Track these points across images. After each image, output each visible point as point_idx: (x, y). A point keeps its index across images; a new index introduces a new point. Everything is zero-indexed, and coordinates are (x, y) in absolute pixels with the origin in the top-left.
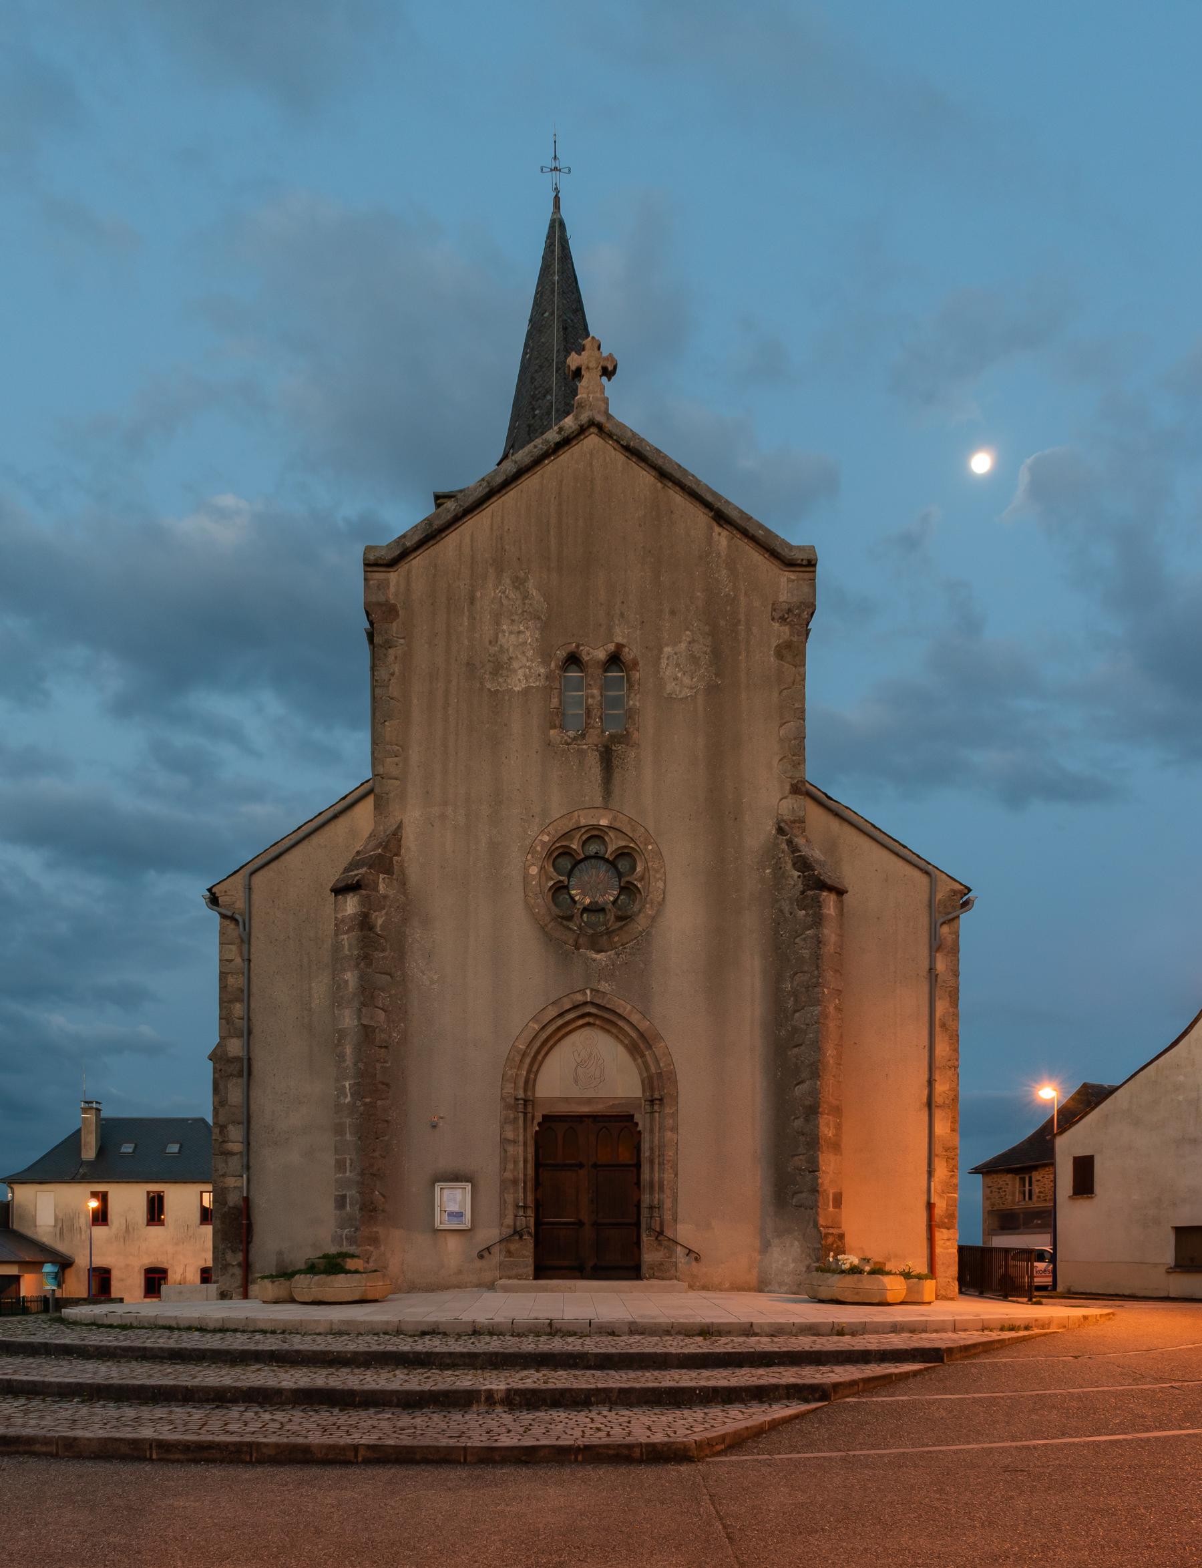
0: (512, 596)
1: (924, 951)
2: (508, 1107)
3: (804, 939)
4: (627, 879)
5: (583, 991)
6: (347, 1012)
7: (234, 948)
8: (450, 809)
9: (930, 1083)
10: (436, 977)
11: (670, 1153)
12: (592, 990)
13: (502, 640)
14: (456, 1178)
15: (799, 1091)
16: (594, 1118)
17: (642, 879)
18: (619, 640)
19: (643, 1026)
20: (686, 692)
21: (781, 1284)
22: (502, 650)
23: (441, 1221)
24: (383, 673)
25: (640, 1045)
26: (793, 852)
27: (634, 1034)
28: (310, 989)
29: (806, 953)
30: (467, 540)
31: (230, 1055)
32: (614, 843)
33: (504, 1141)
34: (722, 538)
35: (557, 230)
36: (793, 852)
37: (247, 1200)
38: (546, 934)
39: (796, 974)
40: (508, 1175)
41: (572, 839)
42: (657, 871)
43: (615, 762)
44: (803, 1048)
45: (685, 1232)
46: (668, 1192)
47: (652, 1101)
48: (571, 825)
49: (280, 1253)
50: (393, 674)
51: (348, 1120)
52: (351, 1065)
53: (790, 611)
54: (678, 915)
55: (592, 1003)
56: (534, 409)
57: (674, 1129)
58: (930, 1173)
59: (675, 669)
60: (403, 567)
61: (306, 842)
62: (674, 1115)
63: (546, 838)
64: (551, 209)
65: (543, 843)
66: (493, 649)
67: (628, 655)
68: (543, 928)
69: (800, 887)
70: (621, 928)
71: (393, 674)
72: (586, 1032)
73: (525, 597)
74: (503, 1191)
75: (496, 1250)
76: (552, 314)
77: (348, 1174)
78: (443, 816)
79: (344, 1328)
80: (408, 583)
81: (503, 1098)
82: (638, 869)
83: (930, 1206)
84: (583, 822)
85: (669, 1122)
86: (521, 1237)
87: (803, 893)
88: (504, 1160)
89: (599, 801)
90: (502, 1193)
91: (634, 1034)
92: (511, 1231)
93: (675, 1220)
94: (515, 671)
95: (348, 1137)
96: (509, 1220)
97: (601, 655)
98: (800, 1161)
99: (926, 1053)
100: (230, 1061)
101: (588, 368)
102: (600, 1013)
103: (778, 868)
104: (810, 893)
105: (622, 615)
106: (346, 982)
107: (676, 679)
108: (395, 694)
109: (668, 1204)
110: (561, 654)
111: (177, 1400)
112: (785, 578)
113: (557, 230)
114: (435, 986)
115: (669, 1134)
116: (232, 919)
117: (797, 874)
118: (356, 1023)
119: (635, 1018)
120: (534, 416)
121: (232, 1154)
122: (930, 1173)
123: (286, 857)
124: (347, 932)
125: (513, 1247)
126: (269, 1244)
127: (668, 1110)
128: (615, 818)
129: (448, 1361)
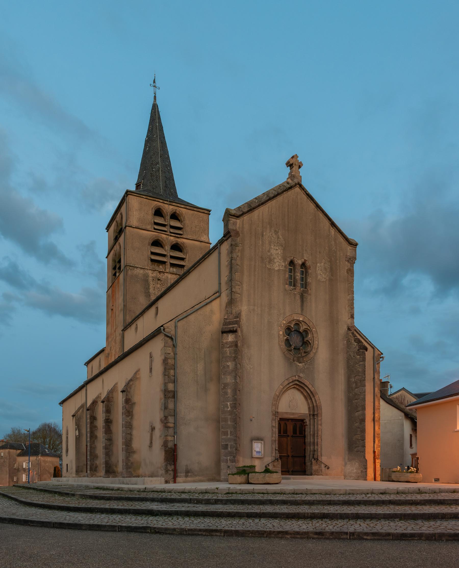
0: (274, 236)
3: (359, 365)
5: (295, 376)
6: (228, 377)
7: (170, 349)
8: (256, 307)
9: (374, 413)
10: (252, 367)
11: (320, 433)
12: (298, 376)
13: (272, 252)
14: (258, 439)
15: (357, 414)
16: (292, 420)
18: (305, 258)
19: (312, 389)
20: (324, 280)
21: (351, 477)
22: (271, 255)
23: (20, 459)
24: (234, 255)
25: (309, 396)
26: (354, 337)
27: (309, 392)
28: (197, 367)
29: (360, 370)
30: (261, 214)
31: (169, 389)
33: (273, 426)
34: (333, 231)
36: (354, 337)
37: (175, 445)
38: (285, 355)
39: (356, 376)
40: (274, 439)
43: (304, 299)
45: (324, 459)
47: (314, 415)
48: (292, 319)
49: (187, 466)
50: (238, 256)
51: (229, 417)
53: (350, 259)
54: (322, 353)
55: (298, 380)
56: (152, 168)
57: (321, 425)
58: (374, 442)
59: (319, 272)
60: (241, 219)
62: (321, 420)
63: (285, 322)
65: (284, 324)
66: (269, 254)
67: (308, 264)
68: (284, 353)
69: (357, 348)
71: (238, 256)
73: (278, 238)
74: (272, 444)
75: (270, 465)
76: (157, 136)
77: (229, 436)
78: (254, 310)
79: (351, 492)
80: (243, 224)
81: (272, 412)
82: (309, 337)
83: (374, 452)
84: (295, 318)
85: (319, 422)
86: (278, 460)
87: (358, 350)
89: (300, 312)
90: (272, 445)
92: (274, 458)
93: (321, 455)
94: (275, 263)
95: (229, 423)
96: (274, 455)
97: (300, 262)
99: (372, 404)
100: (169, 392)
101: (295, 164)
102: (300, 384)
103: (348, 341)
104: (361, 350)
105: (306, 250)
106: (228, 366)
107: (321, 275)
108: (239, 264)
109: (319, 450)
110: (289, 260)
111: (439, 518)
112: (349, 248)
114: (251, 370)
115: (319, 426)
117: (356, 344)
118: (233, 381)
119: (310, 387)
120: (153, 171)
121: (170, 427)
122: (374, 442)
123: (190, 317)
124: (228, 347)
125: (275, 464)
126: (183, 461)
127: (319, 418)
128: (304, 318)
129: (449, 502)
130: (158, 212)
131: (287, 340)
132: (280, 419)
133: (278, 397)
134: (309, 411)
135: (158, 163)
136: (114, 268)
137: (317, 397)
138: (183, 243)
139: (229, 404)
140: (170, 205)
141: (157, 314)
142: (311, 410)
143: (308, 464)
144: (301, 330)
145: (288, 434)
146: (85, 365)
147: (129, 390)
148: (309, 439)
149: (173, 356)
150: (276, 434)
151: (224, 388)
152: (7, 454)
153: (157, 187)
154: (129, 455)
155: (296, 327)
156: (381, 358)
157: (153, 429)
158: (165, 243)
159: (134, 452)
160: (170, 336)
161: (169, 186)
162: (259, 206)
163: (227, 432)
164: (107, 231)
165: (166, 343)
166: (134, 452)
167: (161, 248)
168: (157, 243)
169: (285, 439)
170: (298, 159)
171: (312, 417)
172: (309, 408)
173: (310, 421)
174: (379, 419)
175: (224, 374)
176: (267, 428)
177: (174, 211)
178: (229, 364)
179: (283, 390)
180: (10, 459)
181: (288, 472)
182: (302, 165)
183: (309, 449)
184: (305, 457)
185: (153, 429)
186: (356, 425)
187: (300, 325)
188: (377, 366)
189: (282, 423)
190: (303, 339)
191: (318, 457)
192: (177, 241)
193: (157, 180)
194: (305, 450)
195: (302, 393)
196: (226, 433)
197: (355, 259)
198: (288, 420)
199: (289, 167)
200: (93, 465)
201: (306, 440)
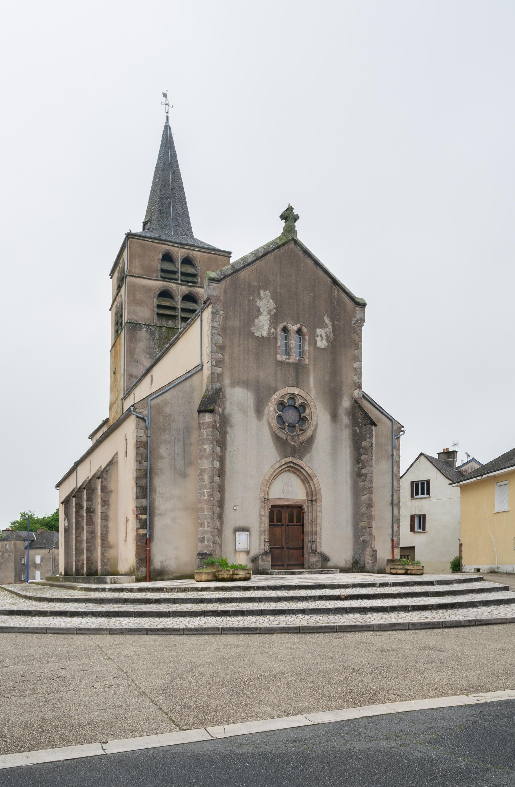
1: (390, 448)
2: (262, 502)
4: (303, 415)
6: (206, 462)
7: (142, 431)
9: (392, 496)
11: (319, 520)
14: (244, 529)
15: (363, 498)
16: (288, 507)
17: (309, 415)
19: (310, 472)
23: (32, 552)
25: (306, 479)
27: (306, 475)
32: (299, 402)
33: (261, 515)
35: (167, 130)
40: (262, 529)
41: (284, 398)
42: (314, 413)
44: (365, 482)
46: (318, 535)
51: (206, 506)
52: (208, 483)
55: (292, 462)
57: (320, 511)
61: (173, 389)
62: (320, 506)
64: (165, 120)
70: (302, 434)
72: (287, 473)
77: (206, 528)
82: (307, 412)
84: (289, 392)
85: (319, 509)
88: (261, 523)
90: (260, 536)
91: (306, 475)
95: (206, 513)
96: (262, 547)
98: (363, 524)
102: (294, 466)
106: (205, 449)
109: (318, 540)
113: (167, 130)
115: (318, 513)
116: (143, 419)
118: (211, 466)
119: (307, 469)
122: (393, 528)
124: (205, 429)
128: (300, 391)
130: (167, 257)
131: (280, 417)
132: (272, 506)
133: (268, 481)
134: (307, 496)
135: (169, 197)
136: (117, 324)
137: (315, 480)
138: (197, 293)
139: (205, 491)
140: (181, 248)
141: (152, 383)
142: (309, 495)
143: (306, 556)
144: (297, 404)
145: (283, 522)
146: (89, 438)
147: (104, 476)
148: (307, 528)
149: (146, 439)
150: (265, 524)
151: (201, 474)
152: (13, 547)
153: (167, 226)
154: (105, 550)
155: (291, 402)
156: (401, 431)
157: (127, 521)
158: (175, 294)
159: (111, 547)
160: (142, 416)
161: (182, 224)
162: (244, 267)
163: (204, 523)
164: (111, 278)
165: (137, 424)
166: (111, 547)
167: (171, 300)
168: (165, 294)
169: (280, 529)
170: (293, 211)
171: (310, 503)
172: (307, 493)
173: (308, 507)
174: (399, 502)
175: (200, 459)
176: (256, 518)
177: (186, 255)
178: (206, 447)
179: (275, 474)
180: (16, 552)
182: (298, 217)
183: (308, 539)
184: (303, 548)
185: (127, 521)
186: (363, 510)
187: (296, 399)
188: (396, 441)
189: (276, 511)
190: (300, 415)
191: (316, 548)
192: (190, 290)
193: (167, 218)
194: (303, 540)
195: (298, 476)
196: (202, 525)
197: (364, 321)
198: (283, 507)
199: (284, 221)
200: (79, 561)
201: (305, 530)
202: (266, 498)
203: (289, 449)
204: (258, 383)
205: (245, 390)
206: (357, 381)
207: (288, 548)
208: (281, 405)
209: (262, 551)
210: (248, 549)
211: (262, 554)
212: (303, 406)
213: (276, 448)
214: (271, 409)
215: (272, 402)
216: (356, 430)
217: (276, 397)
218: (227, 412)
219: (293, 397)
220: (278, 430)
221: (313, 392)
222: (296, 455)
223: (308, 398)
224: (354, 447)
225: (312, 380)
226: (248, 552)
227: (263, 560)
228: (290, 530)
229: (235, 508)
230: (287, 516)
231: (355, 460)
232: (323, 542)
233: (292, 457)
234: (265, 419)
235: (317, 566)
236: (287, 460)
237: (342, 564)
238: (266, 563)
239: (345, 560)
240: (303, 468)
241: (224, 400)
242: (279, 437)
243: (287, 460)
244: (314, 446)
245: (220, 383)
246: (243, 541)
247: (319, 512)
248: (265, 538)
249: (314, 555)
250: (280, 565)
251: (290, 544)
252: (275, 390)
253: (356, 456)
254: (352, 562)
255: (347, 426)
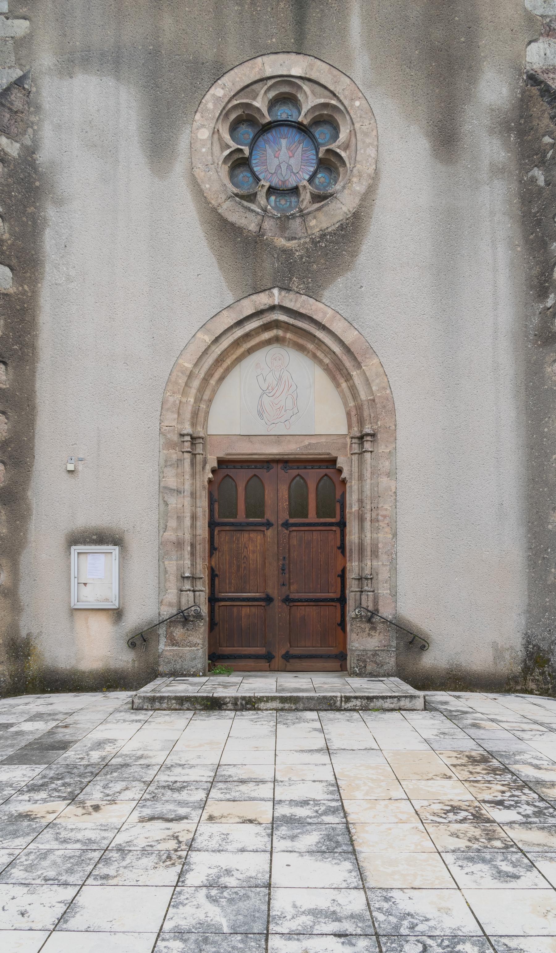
2: (170, 445)
11: (386, 506)
14: (101, 538)
16: (285, 462)
17: (346, 147)
19: (349, 337)
25: (341, 364)
27: (336, 348)
33: (164, 490)
40: (170, 535)
42: (366, 134)
46: (384, 558)
62: (391, 455)
72: (274, 350)
84: (269, 72)
85: (385, 465)
88: (165, 516)
90: (161, 559)
91: (336, 348)
96: (171, 596)
102: (291, 321)
109: (384, 574)
115: (384, 481)
119: (338, 327)
128: (311, 66)
134: (350, 427)
137: (370, 366)
145: (269, 515)
169: (258, 538)
181: (269, 657)
184: (342, 600)
187: (300, 96)
191: (376, 602)
202: (188, 429)
203: (269, 265)
204: (155, 54)
205: (110, 82)
206: (539, 12)
207: (287, 600)
208: (244, 120)
209: (167, 611)
210: (115, 604)
211: (171, 621)
212: (327, 118)
213: (220, 259)
214: (204, 136)
215: (207, 110)
216: (533, 180)
217: (220, 92)
218: (43, 157)
219: (286, 92)
220: (228, 204)
221: (361, 64)
222: (295, 283)
223: (342, 86)
224: (527, 241)
225: (356, 24)
226: (117, 614)
227: (173, 642)
228: (294, 542)
229: (71, 467)
230: (284, 492)
231: (532, 287)
232: (406, 581)
233: (281, 289)
234: (179, 168)
235: (380, 665)
236: (263, 300)
237: (479, 659)
238: (194, 645)
239: (494, 645)
240: (323, 328)
241: (33, 118)
242: (232, 224)
243: (263, 300)
244: (367, 247)
245: (21, 66)
246: (97, 575)
247: (388, 475)
248: (180, 568)
249: (367, 626)
250: (257, 657)
251: (293, 587)
252: (219, 72)
253: (536, 271)
254: (521, 653)
255: (497, 171)
